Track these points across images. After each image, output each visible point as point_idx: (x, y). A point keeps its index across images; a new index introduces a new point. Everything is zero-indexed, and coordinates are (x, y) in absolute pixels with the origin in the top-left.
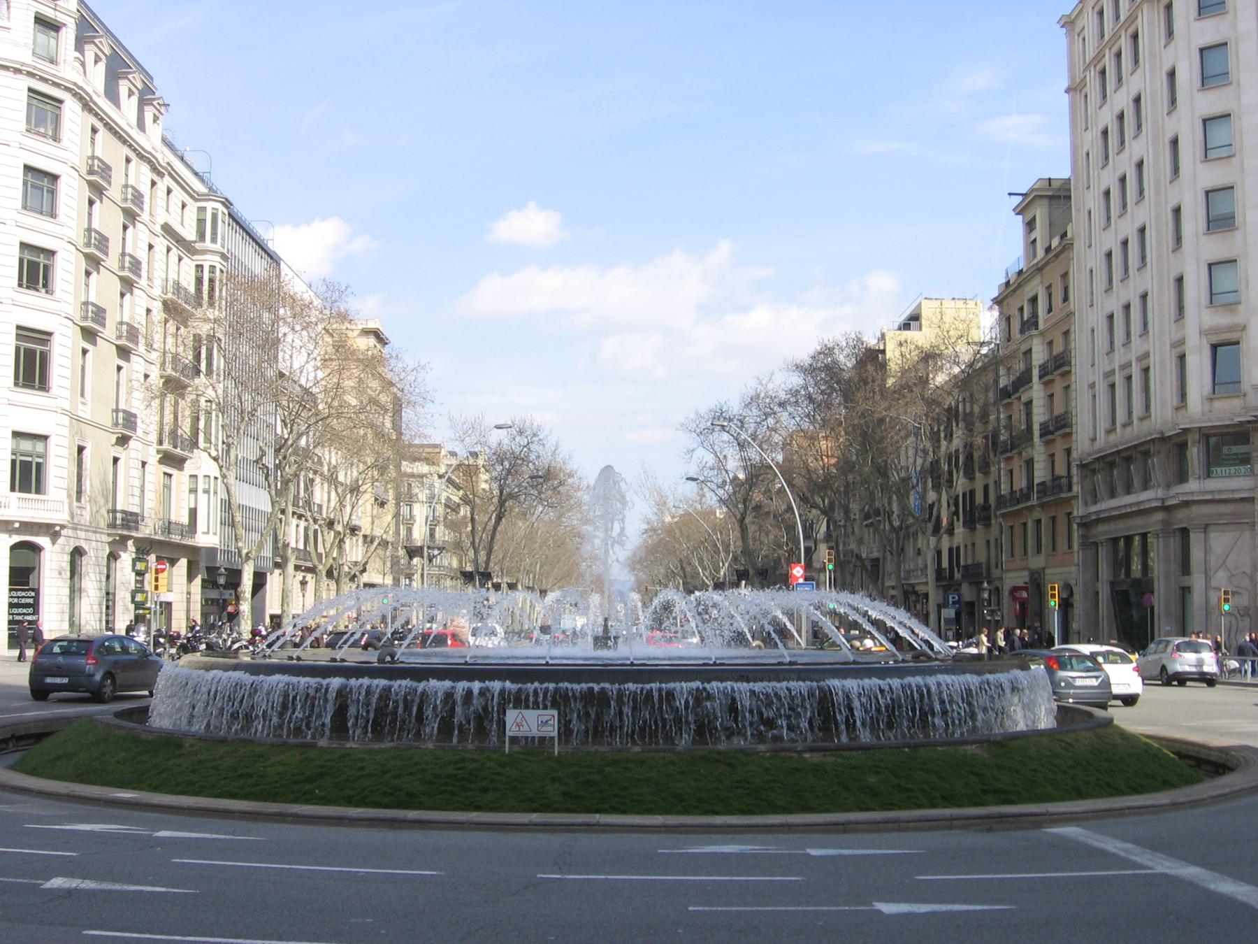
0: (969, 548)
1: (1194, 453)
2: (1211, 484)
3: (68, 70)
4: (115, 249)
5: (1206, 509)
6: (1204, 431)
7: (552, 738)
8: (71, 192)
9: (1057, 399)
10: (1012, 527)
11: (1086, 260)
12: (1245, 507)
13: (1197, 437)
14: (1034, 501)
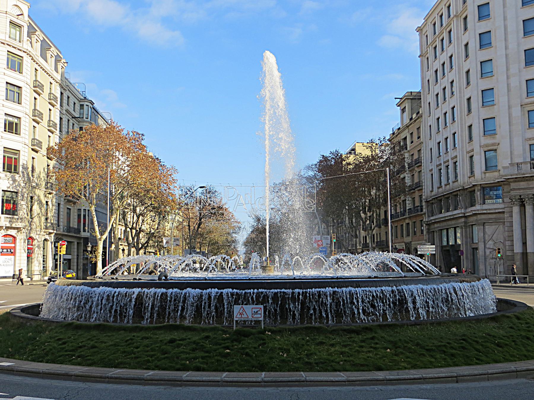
0: (378, 235)
1: (478, 194)
2: (485, 207)
3: (26, 46)
4: (46, 118)
5: (483, 217)
6: (482, 185)
7: (261, 321)
8: (27, 94)
9: (416, 175)
10: (414, 222)
11: (429, 121)
12: (501, 215)
13: (479, 188)
14: (407, 216)
